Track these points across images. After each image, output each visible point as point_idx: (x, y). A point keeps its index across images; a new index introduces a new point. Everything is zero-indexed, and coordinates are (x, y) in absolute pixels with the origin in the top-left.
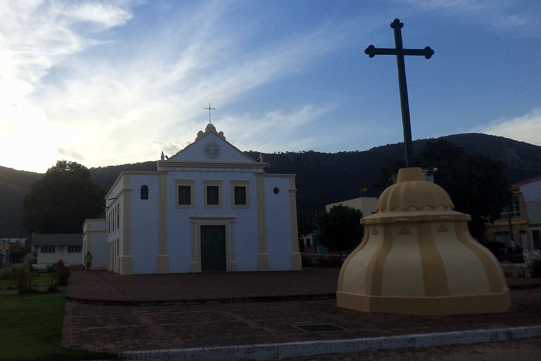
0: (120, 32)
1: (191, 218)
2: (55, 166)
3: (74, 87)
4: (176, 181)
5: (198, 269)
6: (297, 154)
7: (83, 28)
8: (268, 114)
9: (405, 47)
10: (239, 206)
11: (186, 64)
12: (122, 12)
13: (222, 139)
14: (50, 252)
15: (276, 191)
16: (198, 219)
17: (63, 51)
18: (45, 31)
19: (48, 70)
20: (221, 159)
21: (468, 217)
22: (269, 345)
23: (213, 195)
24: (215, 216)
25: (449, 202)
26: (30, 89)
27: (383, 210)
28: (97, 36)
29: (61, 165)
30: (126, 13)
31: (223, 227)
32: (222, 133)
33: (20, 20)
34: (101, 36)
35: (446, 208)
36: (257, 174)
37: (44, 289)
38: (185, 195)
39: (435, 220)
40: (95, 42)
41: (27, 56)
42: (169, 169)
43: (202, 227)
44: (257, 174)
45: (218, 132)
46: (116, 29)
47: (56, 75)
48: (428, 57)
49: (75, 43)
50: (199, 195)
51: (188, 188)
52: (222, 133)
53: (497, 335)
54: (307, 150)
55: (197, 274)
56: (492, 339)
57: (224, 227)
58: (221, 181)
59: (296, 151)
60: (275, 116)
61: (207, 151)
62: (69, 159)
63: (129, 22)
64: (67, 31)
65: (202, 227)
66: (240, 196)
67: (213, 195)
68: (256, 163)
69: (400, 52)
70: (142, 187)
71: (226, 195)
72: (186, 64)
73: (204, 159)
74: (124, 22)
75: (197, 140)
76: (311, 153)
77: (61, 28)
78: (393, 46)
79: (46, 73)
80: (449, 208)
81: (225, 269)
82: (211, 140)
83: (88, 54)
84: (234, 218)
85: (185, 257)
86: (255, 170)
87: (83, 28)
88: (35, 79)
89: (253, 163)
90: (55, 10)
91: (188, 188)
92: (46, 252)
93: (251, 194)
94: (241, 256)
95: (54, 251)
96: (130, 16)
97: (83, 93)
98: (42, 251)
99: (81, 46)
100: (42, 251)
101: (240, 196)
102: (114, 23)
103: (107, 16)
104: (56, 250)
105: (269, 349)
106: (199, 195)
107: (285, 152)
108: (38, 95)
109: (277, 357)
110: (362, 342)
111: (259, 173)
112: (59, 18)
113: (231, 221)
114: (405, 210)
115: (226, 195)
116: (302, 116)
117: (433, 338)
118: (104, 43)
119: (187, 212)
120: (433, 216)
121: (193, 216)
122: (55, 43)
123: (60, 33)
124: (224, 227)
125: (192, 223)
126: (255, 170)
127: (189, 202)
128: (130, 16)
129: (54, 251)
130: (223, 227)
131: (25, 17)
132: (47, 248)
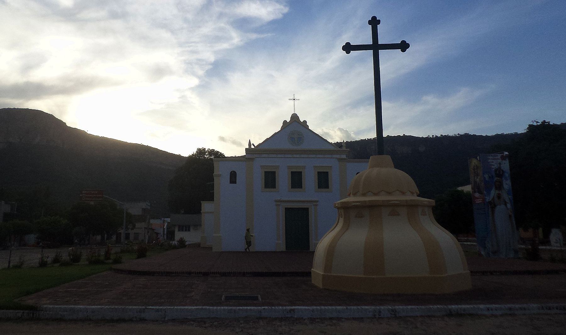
0: (278, 26)
1: (276, 201)
3: (236, 78)
4: (289, 167)
5: (283, 248)
6: (452, 137)
7: (243, 24)
8: (425, 98)
9: (370, 42)
10: (268, 189)
12: (278, 6)
13: (305, 127)
16: (281, 201)
17: (225, 46)
18: (208, 29)
19: (211, 64)
20: (304, 146)
21: (432, 202)
22: (157, 307)
23: (297, 180)
24: (290, 199)
25: (416, 189)
26: (195, 82)
27: (355, 194)
30: (282, 7)
31: (306, 210)
33: (186, 20)
35: (412, 193)
36: (340, 160)
38: (270, 180)
39: (385, 205)
40: (254, 36)
41: (193, 52)
42: (256, 156)
44: (340, 160)
45: (302, 120)
47: (218, 69)
48: (404, 50)
49: (236, 38)
51: (326, 174)
53: (380, 312)
54: (462, 133)
55: (282, 252)
56: (375, 315)
57: (307, 210)
58: (305, 166)
59: (451, 134)
60: (431, 100)
62: (208, 146)
63: (285, 16)
64: (228, 27)
66: (323, 180)
67: (297, 180)
68: (339, 149)
69: (376, 47)
70: (231, 172)
71: (310, 180)
73: (288, 146)
74: (280, 16)
75: (283, 128)
76: (467, 136)
77: (222, 25)
78: (370, 42)
79: (210, 67)
80: (415, 194)
81: (309, 249)
82: (295, 128)
83: (248, 48)
84: (317, 201)
85: (270, 236)
86: (338, 156)
87: (243, 24)
88: (201, 72)
89: (336, 149)
90: (217, 9)
91: (326, 174)
92: (183, 231)
93: (334, 178)
95: (189, 230)
96: (286, 10)
97: (243, 84)
98: (179, 230)
99: (241, 41)
100: (179, 230)
101: (323, 180)
102: (271, 17)
103: (264, 12)
104: (191, 229)
105: (158, 310)
107: (439, 136)
108: (203, 88)
109: (165, 318)
110: (242, 310)
111: (342, 159)
112: (221, 16)
114: (364, 195)
115: (310, 180)
116: (459, 99)
117: (313, 311)
118: (262, 36)
120: (383, 201)
121: (279, 199)
122: (217, 39)
123: (221, 29)
124: (307, 210)
125: (277, 205)
126: (338, 156)
127: (274, 186)
129: (189, 230)
130: (306, 210)
131: (190, 16)
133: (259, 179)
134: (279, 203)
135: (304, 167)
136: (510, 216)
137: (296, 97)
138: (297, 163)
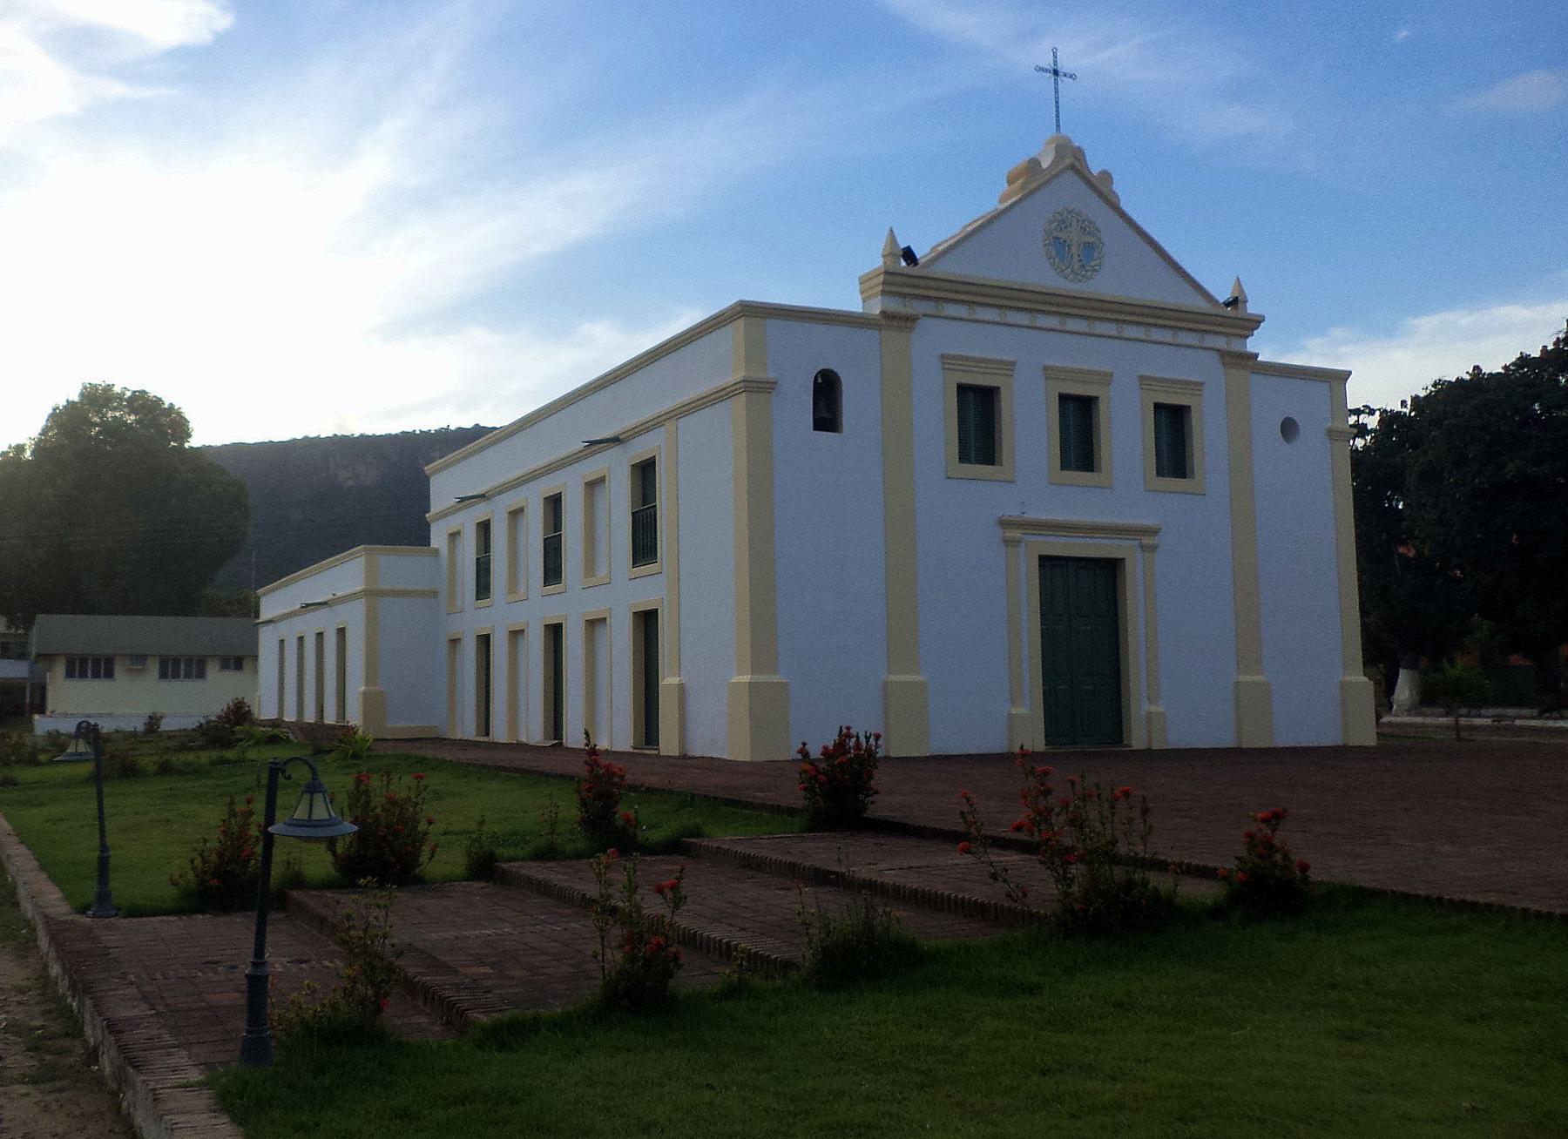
0: (197, 66)
1: (1004, 523)
2: (76, 399)
4: (1050, 373)
5: (1036, 741)
8: (585, 328)
11: (376, 165)
14: (96, 675)
15: (1289, 428)
20: (1104, 285)
28: (122, 73)
29: (97, 397)
32: (1106, 176)
34: (137, 71)
37: (656, 836)
38: (979, 419)
40: (116, 89)
43: (1047, 562)
46: (181, 54)
50: (1029, 427)
52: (1106, 176)
61: (1057, 245)
62: (126, 380)
65: (1047, 562)
71: (1126, 434)
72: (376, 165)
73: (1042, 275)
74: (205, 37)
84: (1153, 532)
94: (1180, 694)
95: (109, 674)
96: (225, 21)
98: (70, 674)
100: (70, 674)
106: (1029, 427)
113: (1147, 541)
115: (1126, 434)
119: (983, 498)
121: (1013, 512)
125: (1006, 541)
128: (225, 21)
129: (109, 674)
130: (1111, 568)
132: (177, 662)
133: (935, 423)
134: (1017, 534)
135: (1106, 378)
136: (130, 670)
137: (1064, 66)
138: (1083, 355)
